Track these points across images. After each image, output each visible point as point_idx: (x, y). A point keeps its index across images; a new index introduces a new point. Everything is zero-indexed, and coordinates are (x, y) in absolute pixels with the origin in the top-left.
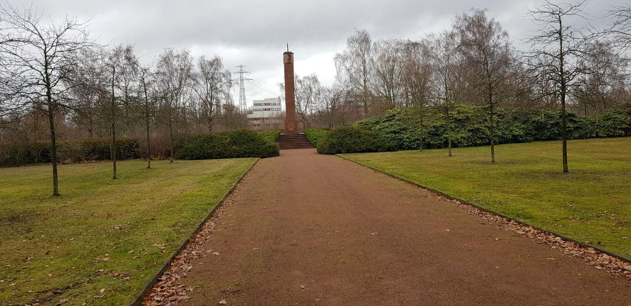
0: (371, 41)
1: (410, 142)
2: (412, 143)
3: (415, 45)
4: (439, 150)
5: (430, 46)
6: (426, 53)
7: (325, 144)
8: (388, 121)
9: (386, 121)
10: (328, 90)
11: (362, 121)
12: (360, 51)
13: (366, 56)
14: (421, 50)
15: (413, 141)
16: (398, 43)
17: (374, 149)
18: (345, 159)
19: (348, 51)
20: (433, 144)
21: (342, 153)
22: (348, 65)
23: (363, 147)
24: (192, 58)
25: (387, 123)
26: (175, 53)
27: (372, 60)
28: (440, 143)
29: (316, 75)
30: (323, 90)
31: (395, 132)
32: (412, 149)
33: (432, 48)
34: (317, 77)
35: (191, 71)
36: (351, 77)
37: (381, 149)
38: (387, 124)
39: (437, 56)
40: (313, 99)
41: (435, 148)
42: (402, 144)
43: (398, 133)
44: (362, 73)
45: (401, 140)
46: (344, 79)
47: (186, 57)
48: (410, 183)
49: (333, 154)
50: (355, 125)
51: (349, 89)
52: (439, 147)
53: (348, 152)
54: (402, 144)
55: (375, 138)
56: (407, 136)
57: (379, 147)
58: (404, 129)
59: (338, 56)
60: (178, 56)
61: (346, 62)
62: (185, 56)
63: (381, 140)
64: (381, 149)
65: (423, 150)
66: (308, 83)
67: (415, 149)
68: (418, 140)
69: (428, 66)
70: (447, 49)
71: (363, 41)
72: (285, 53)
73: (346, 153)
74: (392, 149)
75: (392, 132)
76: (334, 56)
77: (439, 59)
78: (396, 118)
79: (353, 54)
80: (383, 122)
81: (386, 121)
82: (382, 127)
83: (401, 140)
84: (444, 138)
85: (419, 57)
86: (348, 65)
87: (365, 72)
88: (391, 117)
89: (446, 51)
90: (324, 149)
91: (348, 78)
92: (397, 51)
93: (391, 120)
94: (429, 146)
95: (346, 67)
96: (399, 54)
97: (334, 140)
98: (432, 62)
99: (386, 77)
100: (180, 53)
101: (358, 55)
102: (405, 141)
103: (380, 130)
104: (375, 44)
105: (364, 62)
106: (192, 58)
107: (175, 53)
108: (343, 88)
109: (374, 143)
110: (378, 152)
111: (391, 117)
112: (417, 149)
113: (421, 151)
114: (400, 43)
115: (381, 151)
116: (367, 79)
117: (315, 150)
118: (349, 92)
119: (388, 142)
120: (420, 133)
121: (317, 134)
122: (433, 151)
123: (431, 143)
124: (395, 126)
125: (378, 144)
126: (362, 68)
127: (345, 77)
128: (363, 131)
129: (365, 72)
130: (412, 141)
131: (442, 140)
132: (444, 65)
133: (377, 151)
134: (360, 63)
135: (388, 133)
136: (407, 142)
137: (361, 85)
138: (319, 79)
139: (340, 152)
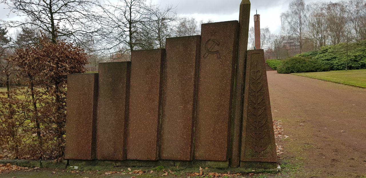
0: (305, 4)
1: (338, 66)
2: (340, 66)
3: (335, 5)
4: (358, 70)
5: (345, 5)
6: (343, 10)
7: (283, 67)
8: (323, 53)
9: (321, 53)
10: (276, 36)
11: (301, 54)
12: (297, 11)
13: (301, 13)
14: (338, 8)
15: (340, 65)
16: (323, 4)
17: (315, 70)
18: (298, 76)
19: (290, 11)
20: (353, 67)
21: (294, 73)
22: (289, 20)
23: (308, 69)
24: (197, 22)
25: (322, 54)
26: (187, 20)
27: (305, 16)
28: (358, 66)
29: (268, 27)
30: (273, 36)
31: (328, 60)
32: (339, 70)
33: (346, 6)
34: (269, 28)
35: (195, 29)
36: (291, 28)
37: (319, 70)
38: (322, 55)
39: (350, 11)
40: (266, 42)
41: (355, 69)
42: (333, 67)
43: (330, 60)
44: (299, 25)
45: (332, 64)
46: (286, 29)
47: (193, 22)
48: (353, 86)
49: (288, 73)
50: (297, 56)
51: (289, 35)
52: (357, 69)
53: (298, 72)
54: (333, 67)
55: (315, 64)
56: (336, 62)
57: (318, 69)
58: (335, 58)
59: (283, 14)
60: (189, 21)
61: (288, 18)
62: (193, 21)
63: (319, 65)
64: (319, 70)
65: (348, 70)
66: (263, 32)
67: (341, 70)
68: (343, 64)
69: (343, 18)
70: (357, 6)
71: (299, 4)
72: (255, 15)
73: (297, 72)
74: (326, 70)
75: (326, 60)
76: (280, 15)
77: (351, 13)
78: (328, 51)
79: (293, 13)
80: (320, 54)
81: (321, 53)
82: (319, 57)
83: (332, 64)
84: (361, 63)
85: (337, 11)
86: (289, 20)
87: (301, 24)
88: (325, 50)
89: (357, 7)
90: (282, 71)
91: (289, 28)
92: (322, 9)
93: (325, 53)
94: (350, 68)
95: (288, 21)
96: (324, 11)
97: (289, 65)
98: (346, 15)
99: (317, 25)
100: (190, 19)
101: (296, 13)
102: (335, 65)
103: (318, 58)
104: (308, 6)
105: (300, 17)
106: (197, 22)
107: (187, 20)
108: (285, 34)
109: (314, 66)
110: (317, 72)
111: (325, 50)
112: (342, 70)
113: (346, 71)
114: (324, 4)
115: (319, 71)
116: (302, 28)
117: (276, 71)
118: (289, 37)
119: (324, 66)
120: (344, 59)
121: (275, 62)
122: (354, 70)
123: (352, 66)
124: (328, 56)
125: (318, 67)
126: (299, 22)
127: (287, 27)
128: (307, 60)
129: (301, 24)
130: (339, 65)
131: (359, 64)
132: (355, 16)
133: (316, 71)
134: (297, 18)
135: (323, 61)
136: (336, 65)
137: (298, 32)
138: (270, 29)
139: (292, 72)
